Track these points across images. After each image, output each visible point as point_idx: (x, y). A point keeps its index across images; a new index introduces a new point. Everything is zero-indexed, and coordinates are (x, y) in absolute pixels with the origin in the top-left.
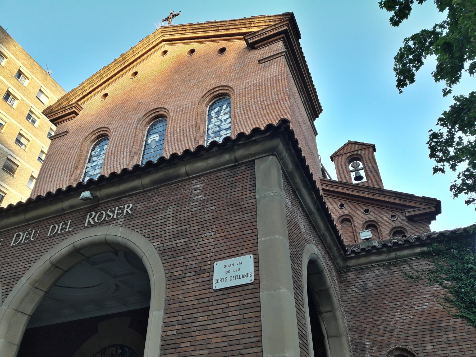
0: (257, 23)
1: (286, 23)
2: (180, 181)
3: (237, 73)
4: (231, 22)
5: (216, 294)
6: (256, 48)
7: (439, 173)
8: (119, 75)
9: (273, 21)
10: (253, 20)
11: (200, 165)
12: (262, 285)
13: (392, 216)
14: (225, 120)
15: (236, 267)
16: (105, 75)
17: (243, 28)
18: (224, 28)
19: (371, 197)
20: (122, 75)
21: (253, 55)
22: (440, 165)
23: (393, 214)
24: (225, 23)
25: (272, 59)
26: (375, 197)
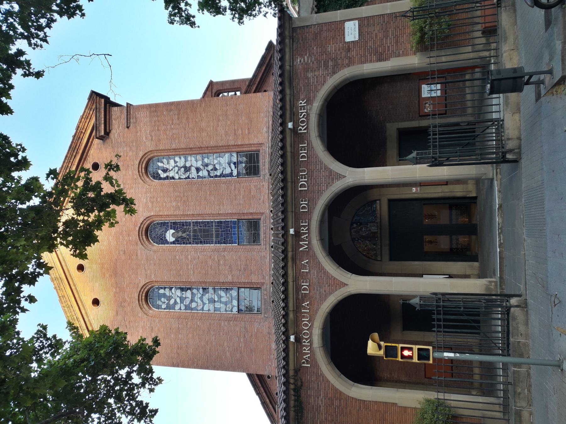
0: (84, 126)
1: (98, 99)
2: (293, 73)
3: (131, 149)
4: (70, 152)
5: (360, 39)
6: (110, 131)
7: (267, 15)
8: (73, 288)
9: (90, 111)
10: (80, 129)
11: (287, 57)
12: (359, 16)
13: (273, 75)
14: (176, 162)
15: (350, 30)
16: (69, 303)
17: (81, 141)
18: (72, 161)
19: (256, 85)
20: (75, 285)
21: (116, 135)
22: (263, 13)
23: (272, 74)
24: (68, 158)
25: (129, 116)
26: (257, 83)
